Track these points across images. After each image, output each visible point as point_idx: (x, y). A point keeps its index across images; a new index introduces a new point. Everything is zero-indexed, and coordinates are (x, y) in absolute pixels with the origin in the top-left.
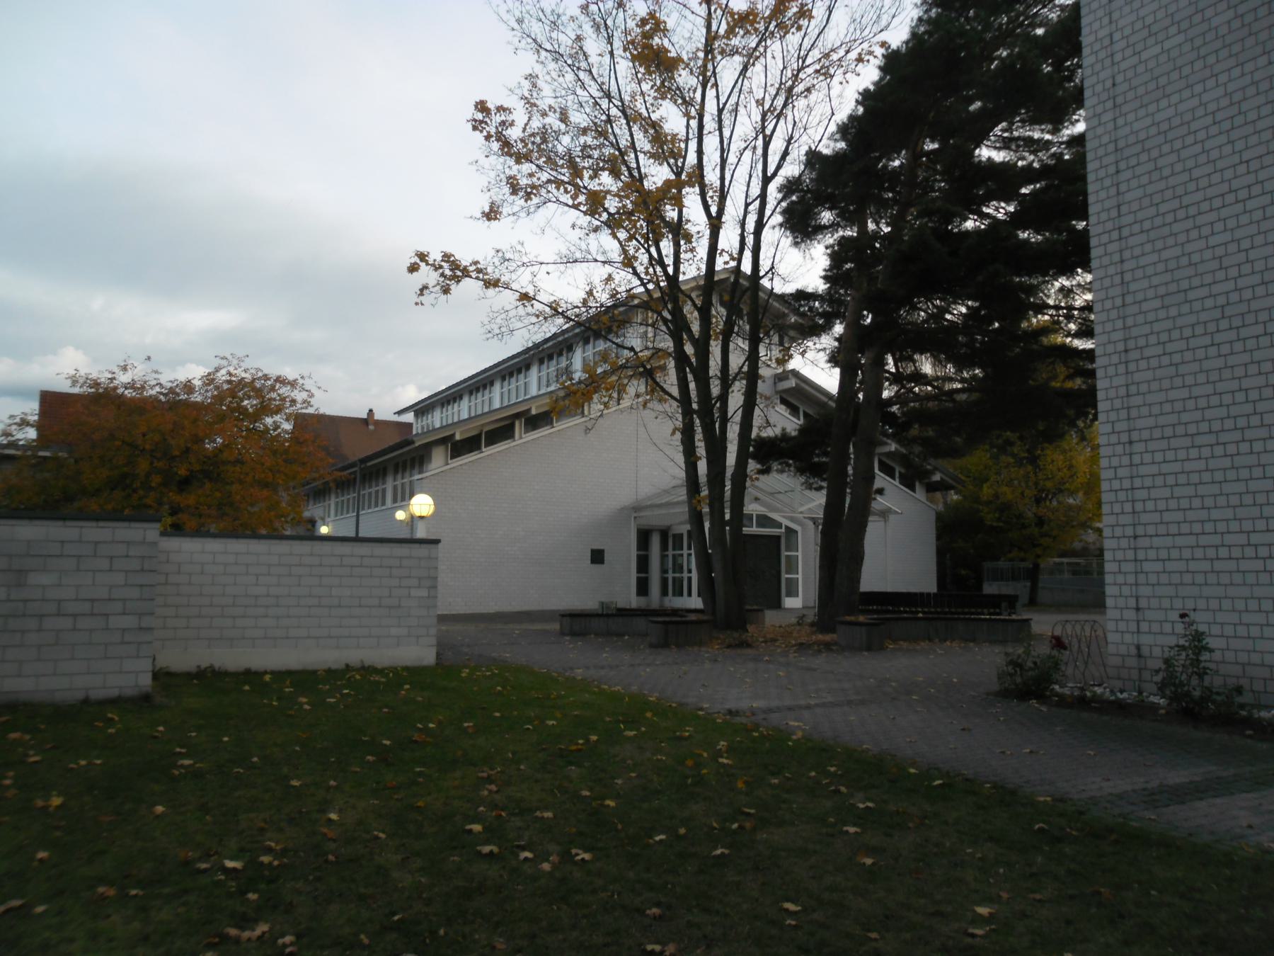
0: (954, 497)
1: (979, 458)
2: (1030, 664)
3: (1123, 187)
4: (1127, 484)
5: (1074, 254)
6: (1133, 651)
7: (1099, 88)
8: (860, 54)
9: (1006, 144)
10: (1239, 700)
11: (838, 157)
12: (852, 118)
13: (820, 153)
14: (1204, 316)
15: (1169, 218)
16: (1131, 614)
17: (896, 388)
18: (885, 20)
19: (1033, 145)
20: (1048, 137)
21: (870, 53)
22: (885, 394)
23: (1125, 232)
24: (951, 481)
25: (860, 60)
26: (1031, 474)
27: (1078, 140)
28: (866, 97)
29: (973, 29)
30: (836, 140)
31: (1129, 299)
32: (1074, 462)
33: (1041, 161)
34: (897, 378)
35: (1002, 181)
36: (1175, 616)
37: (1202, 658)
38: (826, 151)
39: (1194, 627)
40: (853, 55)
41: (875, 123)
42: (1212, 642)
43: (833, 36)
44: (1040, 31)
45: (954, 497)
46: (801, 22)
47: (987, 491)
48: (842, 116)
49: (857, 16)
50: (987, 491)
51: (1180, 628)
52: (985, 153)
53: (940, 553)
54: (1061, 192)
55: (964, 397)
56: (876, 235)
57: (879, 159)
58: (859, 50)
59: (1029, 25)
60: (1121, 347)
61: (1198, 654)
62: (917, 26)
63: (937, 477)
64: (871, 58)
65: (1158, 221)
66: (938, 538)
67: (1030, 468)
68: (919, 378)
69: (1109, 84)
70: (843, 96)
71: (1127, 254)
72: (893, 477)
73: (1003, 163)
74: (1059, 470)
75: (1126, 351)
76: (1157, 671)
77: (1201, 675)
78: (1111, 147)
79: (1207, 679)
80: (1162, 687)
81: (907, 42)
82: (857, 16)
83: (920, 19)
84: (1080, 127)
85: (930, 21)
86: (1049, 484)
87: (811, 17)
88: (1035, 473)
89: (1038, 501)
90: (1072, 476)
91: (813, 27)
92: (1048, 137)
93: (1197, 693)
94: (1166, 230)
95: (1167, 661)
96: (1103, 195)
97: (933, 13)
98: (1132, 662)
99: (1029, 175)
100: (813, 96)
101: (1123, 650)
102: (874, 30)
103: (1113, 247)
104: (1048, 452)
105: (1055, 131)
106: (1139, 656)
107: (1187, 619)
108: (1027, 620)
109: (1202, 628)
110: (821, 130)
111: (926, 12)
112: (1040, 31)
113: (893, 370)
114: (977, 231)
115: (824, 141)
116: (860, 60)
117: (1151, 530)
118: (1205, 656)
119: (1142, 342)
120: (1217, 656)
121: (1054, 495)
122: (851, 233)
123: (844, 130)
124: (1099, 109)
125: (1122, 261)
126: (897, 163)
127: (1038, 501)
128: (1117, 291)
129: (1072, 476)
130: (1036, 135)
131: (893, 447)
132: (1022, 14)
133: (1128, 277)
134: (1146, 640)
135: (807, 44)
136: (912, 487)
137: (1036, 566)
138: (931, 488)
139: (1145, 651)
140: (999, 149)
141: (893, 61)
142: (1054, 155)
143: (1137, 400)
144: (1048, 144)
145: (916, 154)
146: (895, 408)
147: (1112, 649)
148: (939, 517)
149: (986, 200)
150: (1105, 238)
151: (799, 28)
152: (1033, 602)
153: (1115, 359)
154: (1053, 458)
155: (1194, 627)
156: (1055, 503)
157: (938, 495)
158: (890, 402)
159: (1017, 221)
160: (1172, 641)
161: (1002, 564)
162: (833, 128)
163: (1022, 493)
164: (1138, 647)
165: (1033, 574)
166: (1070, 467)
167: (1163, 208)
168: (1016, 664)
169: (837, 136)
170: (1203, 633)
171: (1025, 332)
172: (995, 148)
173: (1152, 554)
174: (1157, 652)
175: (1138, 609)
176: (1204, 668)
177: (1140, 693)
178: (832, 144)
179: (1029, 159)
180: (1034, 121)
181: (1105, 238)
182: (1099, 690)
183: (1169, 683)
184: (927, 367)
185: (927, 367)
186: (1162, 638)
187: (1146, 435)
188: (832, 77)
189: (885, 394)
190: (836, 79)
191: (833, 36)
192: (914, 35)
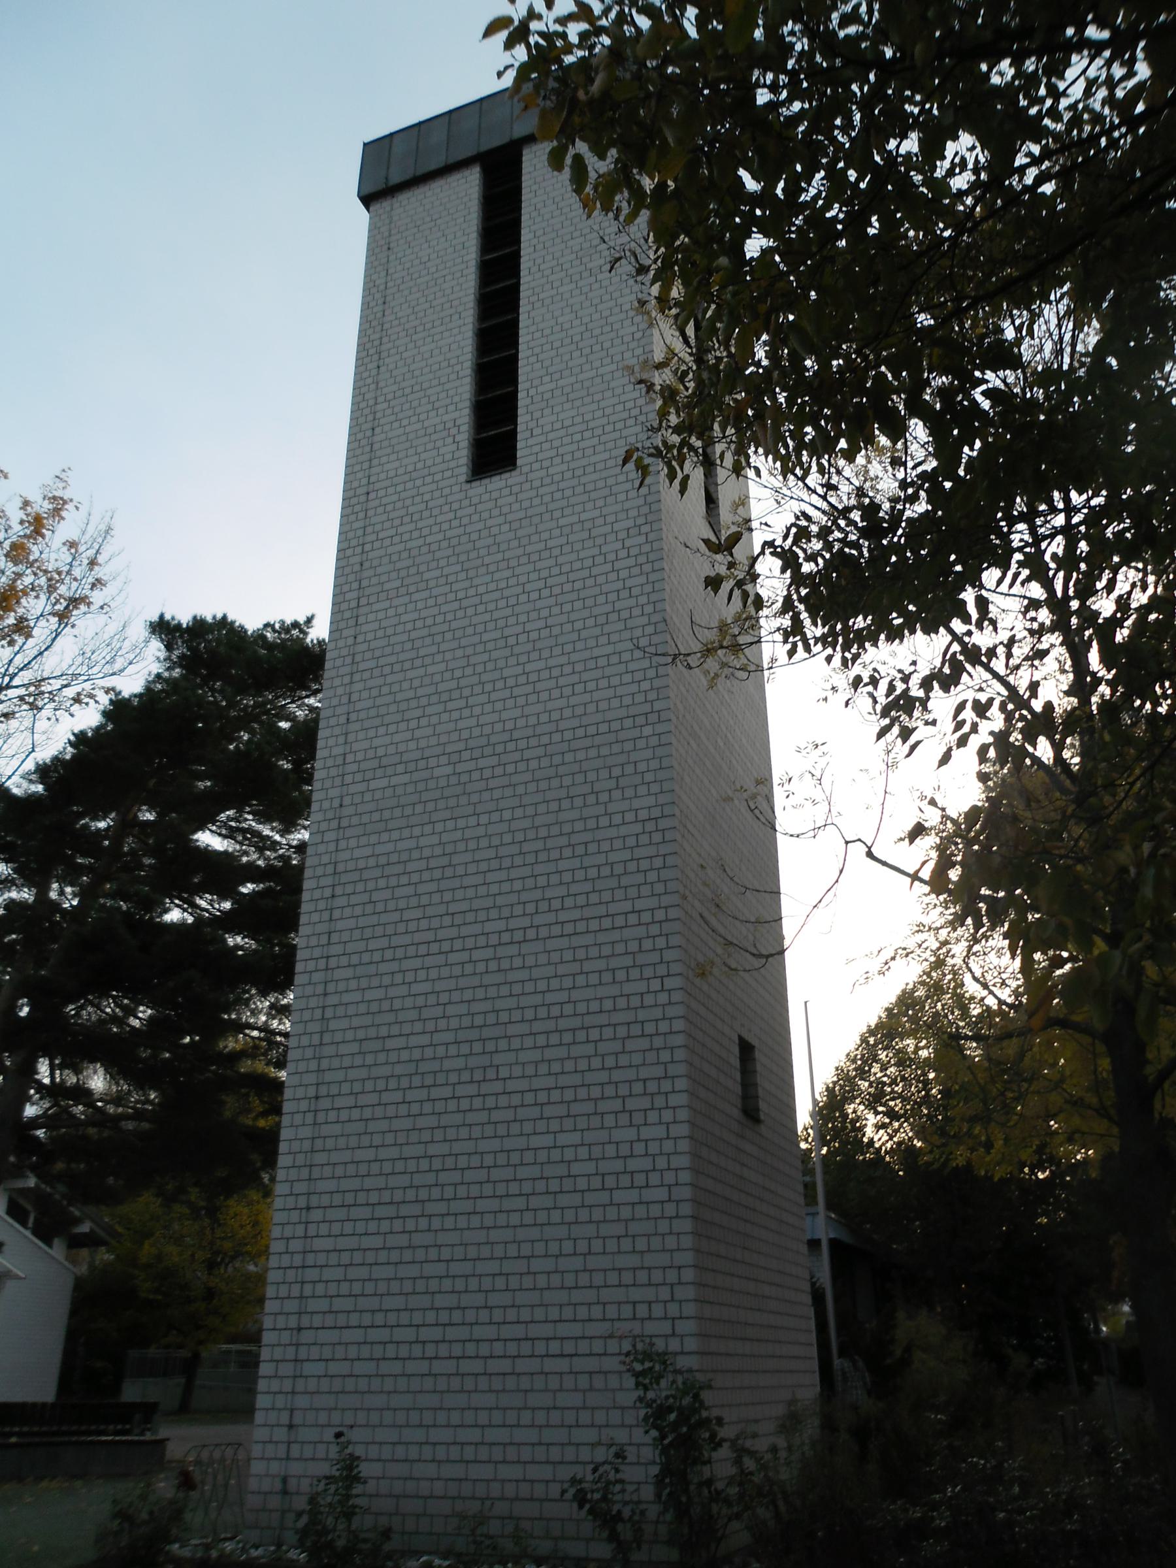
0: (104, 1256)
1: (146, 1203)
2: (144, 1516)
3: (337, 914)
4: (298, 1260)
5: (276, 973)
6: (278, 1486)
7: (326, 805)
8: (79, 694)
9: (230, 834)
10: (387, 1547)
11: (30, 800)
12: (56, 759)
13: (7, 790)
14: (399, 1069)
15: (377, 956)
16: (281, 1434)
17: (47, 1105)
18: (119, 663)
19: (263, 844)
20: (277, 838)
21: (91, 696)
22: (30, 1111)
23: (333, 962)
24: (102, 1234)
25: (77, 700)
26: (208, 1231)
27: (301, 848)
28: (80, 739)
29: (216, 703)
30: (31, 781)
31: (327, 1038)
32: (260, 1218)
33: (267, 859)
34: (53, 1092)
35: (220, 873)
36: (329, 1435)
37: (354, 1492)
38: (16, 791)
39: (348, 1451)
40: (70, 692)
41: (82, 773)
42: (365, 1469)
43: (51, 664)
44: (284, 725)
45: (104, 1256)
46: (16, 637)
47: (147, 1251)
48: (45, 754)
49: (88, 650)
50: (147, 1251)
51: (334, 1450)
52: (209, 839)
53: (72, 1336)
54: (275, 904)
55: (130, 1125)
56: (55, 906)
57: (81, 816)
58: (78, 689)
59: (275, 715)
60: (311, 1092)
61: (349, 1487)
62: (154, 682)
63: (85, 1228)
64: (92, 702)
65: (366, 958)
66: (74, 1312)
67: (207, 1221)
68: (82, 1093)
69: (336, 803)
70: (54, 735)
71: (331, 988)
72: (24, 1223)
73: (226, 852)
74: (242, 1227)
75: (317, 1098)
76: (299, 1514)
77: (349, 1515)
78: (330, 869)
79: (356, 1523)
80: (304, 1533)
81: (140, 696)
82: (88, 650)
83: (158, 676)
84: (305, 835)
85: (166, 681)
86: (228, 1245)
87: (29, 635)
88: (213, 1229)
89: (211, 1266)
90: (255, 1236)
91: (32, 646)
92: (277, 838)
93: (341, 1543)
94: (372, 969)
95: (312, 1500)
96: (315, 917)
97: (177, 673)
98: (274, 1502)
99: (251, 873)
100: (13, 723)
101: (266, 1486)
102: (105, 670)
103: (317, 977)
104: (231, 1202)
105: (284, 832)
106: (285, 1492)
107: (342, 1439)
108: (162, 1442)
109: (359, 1451)
110: (15, 763)
111: (168, 669)
112: (284, 725)
113: (47, 1081)
114: (182, 925)
115: (15, 779)
116: (77, 700)
117: (317, 1321)
118: (358, 1489)
119: (334, 1090)
120: (371, 1487)
121: (233, 1258)
122: (26, 895)
123: (43, 772)
124: (324, 826)
125: (325, 995)
126: (102, 825)
127: (211, 1266)
128: (314, 1027)
129: (255, 1236)
130: (267, 832)
131: (32, 1182)
132: (271, 702)
133: (329, 1013)
134: (295, 1468)
135: (19, 661)
136: (47, 1240)
137: (196, 1356)
138: (76, 1243)
139: (292, 1484)
140: (225, 837)
141: (119, 709)
142: (281, 856)
143: (320, 1158)
144: (275, 845)
145: (127, 824)
146: (40, 1133)
147: (253, 1484)
148: (79, 1284)
149: (201, 890)
150: (311, 965)
151: (11, 643)
152: (184, 1410)
153: (304, 1105)
154: (237, 1209)
155: (348, 1451)
156: (230, 1269)
157: (84, 1253)
158: (34, 1122)
159: (228, 922)
160: (325, 1469)
161: (153, 1351)
162: (30, 765)
163: (193, 1255)
164: (285, 1480)
165: (190, 1367)
166: (256, 1223)
167: (373, 945)
168: (124, 1515)
169: (34, 777)
170: (358, 1458)
171: (220, 1054)
172: (220, 835)
173: (315, 1352)
174: (305, 1486)
175: (291, 1426)
176: (354, 1507)
177: (279, 1546)
178: (25, 784)
179: (252, 857)
180: (263, 817)
181: (311, 965)
182: (229, 1546)
183: (314, 1536)
184: (98, 1082)
185: (98, 1082)
186: (312, 1466)
187: (325, 1200)
188: (40, 709)
189: (30, 1111)
190: (44, 713)
191: (51, 664)
192: (148, 689)
